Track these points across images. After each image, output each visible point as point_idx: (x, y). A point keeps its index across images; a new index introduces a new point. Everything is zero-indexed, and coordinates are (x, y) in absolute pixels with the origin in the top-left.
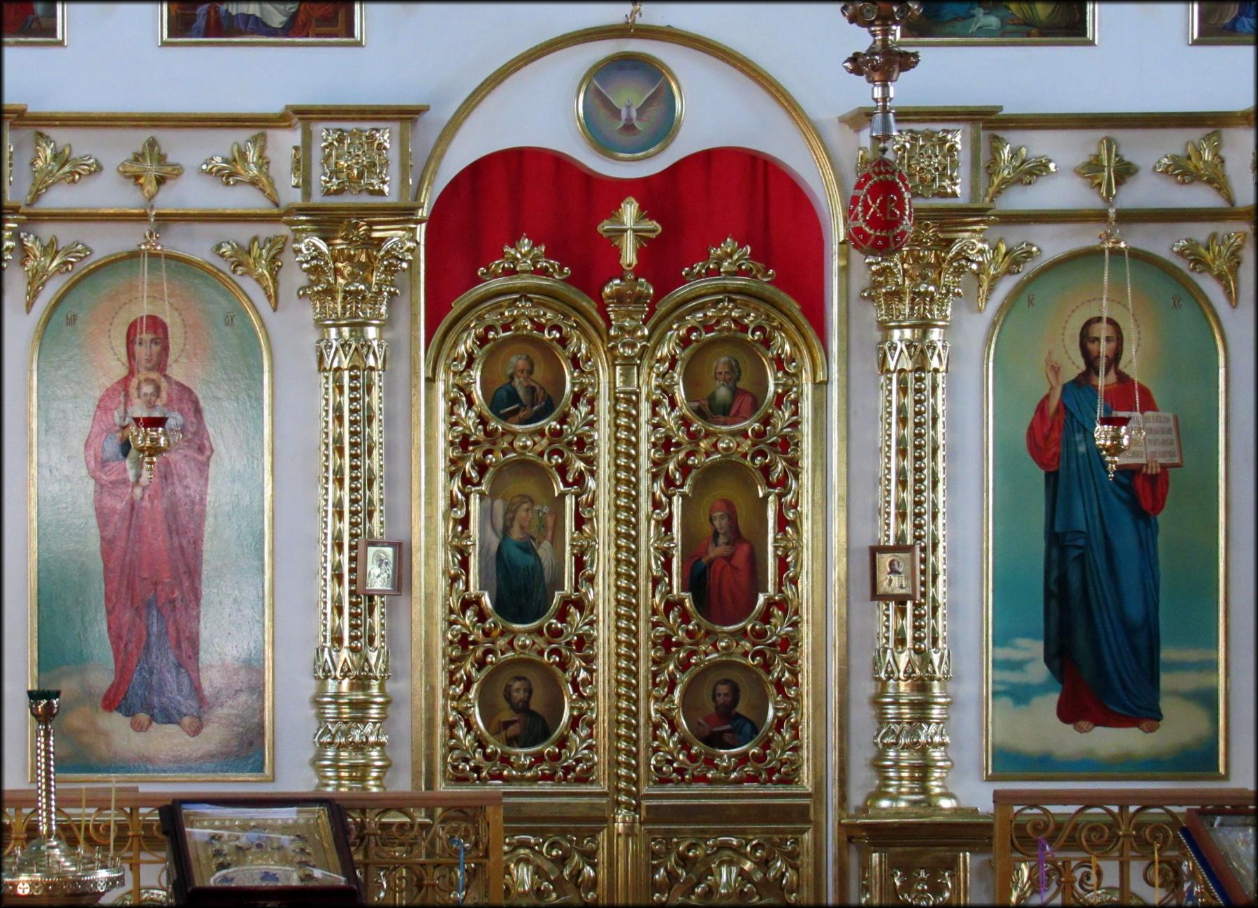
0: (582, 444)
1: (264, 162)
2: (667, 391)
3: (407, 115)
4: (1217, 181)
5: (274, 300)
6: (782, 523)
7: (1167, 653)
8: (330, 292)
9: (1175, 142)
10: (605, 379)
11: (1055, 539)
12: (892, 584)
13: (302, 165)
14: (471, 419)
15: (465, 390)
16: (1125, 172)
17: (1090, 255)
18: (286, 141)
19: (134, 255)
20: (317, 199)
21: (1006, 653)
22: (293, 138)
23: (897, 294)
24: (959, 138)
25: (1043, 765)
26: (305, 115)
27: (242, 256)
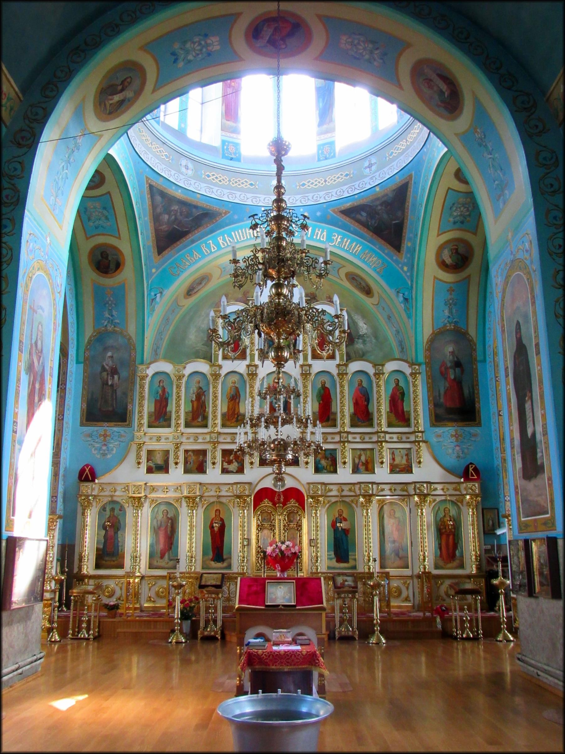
0: (274, 526)
1: (354, 489)
2: (285, 519)
3: (250, 483)
4: (355, 492)
5: (357, 507)
6: (300, 536)
7: (350, 554)
8: (240, 506)
9: (349, 486)
10: (277, 518)
11: (335, 538)
12: (313, 544)
13: (360, 489)
14: (285, 522)
15: (259, 519)
16: (343, 490)
17: (336, 502)
18: (357, 486)
19: (213, 502)
20: (311, 494)
21: (329, 553)
22: (358, 486)
23: (313, 506)
24: (319, 486)
25: (334, 568)
26: (360, 483)
27: (352, 501)
